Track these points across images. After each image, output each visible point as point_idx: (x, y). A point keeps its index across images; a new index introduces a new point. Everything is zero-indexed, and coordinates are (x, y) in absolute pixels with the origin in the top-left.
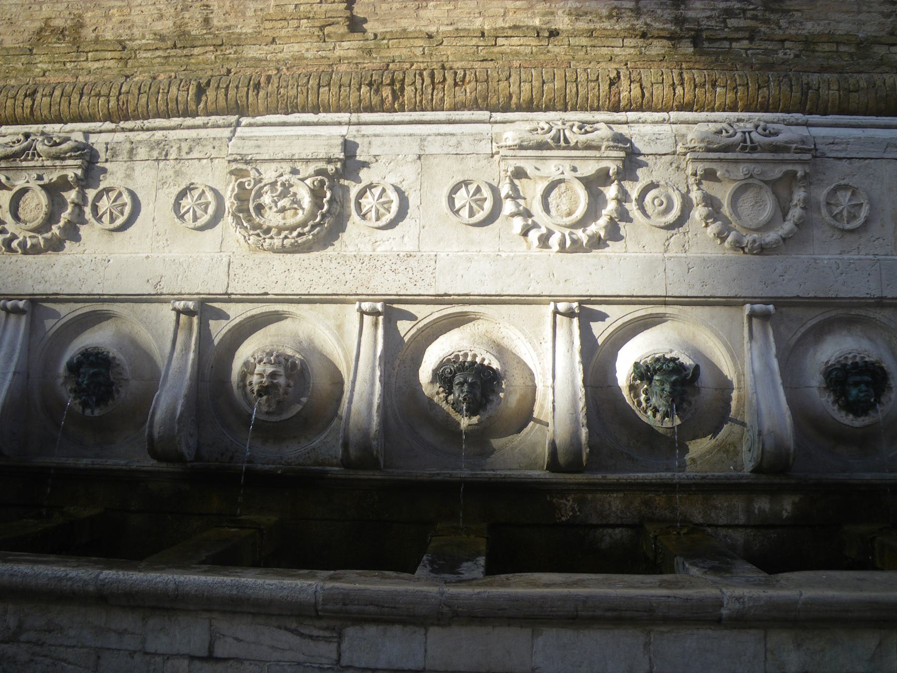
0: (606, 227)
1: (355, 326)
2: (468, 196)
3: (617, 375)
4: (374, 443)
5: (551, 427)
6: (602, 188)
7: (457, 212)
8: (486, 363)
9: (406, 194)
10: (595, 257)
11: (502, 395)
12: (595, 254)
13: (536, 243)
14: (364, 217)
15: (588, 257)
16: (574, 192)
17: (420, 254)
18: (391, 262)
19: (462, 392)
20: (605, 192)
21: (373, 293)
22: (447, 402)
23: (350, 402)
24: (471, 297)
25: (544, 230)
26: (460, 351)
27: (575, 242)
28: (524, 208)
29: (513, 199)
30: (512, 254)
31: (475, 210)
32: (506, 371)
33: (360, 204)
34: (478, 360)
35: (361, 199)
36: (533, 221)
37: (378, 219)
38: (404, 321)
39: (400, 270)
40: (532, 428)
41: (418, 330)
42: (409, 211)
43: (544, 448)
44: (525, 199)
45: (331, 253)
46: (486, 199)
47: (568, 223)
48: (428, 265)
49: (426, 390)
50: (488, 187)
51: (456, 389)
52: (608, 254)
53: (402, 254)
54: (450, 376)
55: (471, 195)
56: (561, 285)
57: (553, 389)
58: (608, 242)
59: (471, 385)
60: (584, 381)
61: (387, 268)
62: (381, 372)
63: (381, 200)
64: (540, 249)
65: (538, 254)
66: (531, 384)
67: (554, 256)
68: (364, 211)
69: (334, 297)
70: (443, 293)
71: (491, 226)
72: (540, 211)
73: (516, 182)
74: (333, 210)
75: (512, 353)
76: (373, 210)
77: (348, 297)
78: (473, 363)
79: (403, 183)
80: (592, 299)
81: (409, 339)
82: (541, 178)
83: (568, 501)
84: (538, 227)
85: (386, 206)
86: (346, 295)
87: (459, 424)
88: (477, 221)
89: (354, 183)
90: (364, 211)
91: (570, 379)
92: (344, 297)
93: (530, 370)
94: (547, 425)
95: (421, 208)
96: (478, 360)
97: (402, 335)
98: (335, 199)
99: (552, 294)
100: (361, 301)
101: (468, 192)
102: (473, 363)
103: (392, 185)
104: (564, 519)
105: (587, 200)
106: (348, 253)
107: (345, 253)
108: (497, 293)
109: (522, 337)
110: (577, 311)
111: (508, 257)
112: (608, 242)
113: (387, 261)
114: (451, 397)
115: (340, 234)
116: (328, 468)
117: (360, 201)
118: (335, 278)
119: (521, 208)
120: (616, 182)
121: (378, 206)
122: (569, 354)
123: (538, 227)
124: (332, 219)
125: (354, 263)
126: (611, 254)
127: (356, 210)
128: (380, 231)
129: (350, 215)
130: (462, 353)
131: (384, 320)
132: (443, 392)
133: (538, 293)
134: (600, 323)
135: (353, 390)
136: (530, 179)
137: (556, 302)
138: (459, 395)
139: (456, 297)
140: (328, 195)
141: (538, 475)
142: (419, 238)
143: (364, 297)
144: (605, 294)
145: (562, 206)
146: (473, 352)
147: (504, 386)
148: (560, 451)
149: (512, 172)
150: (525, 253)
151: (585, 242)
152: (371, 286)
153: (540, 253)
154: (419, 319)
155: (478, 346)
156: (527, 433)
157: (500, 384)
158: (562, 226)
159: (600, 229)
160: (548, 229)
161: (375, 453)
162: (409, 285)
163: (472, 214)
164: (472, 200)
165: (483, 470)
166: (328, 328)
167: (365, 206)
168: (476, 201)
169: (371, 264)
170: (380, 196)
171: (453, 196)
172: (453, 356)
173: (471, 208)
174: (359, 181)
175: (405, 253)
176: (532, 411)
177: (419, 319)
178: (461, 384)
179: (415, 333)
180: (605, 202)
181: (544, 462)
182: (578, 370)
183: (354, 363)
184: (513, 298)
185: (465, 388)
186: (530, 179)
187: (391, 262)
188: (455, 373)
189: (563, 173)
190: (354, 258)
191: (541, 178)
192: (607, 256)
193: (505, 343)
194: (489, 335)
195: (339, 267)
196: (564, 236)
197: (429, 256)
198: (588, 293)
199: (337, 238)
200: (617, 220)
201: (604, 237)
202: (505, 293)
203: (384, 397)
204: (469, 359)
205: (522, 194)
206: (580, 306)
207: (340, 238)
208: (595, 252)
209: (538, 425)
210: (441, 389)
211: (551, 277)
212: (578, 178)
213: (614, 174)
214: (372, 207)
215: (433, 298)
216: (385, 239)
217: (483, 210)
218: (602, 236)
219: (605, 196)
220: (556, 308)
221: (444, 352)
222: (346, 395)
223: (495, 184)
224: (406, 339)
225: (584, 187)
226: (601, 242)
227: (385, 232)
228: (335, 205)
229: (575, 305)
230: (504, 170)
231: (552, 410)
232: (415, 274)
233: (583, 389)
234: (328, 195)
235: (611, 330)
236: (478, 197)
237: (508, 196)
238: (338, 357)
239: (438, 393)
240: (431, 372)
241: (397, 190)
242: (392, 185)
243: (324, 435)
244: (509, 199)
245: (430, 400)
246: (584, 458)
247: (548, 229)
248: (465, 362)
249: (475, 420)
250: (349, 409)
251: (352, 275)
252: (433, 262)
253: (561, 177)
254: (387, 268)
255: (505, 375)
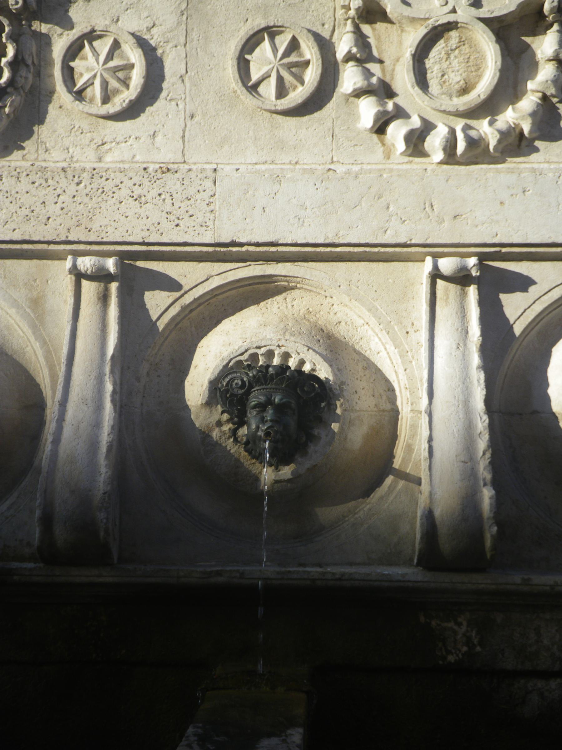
0: (533, 115)
1: (65, 301)
2: (275, 56)
3: (551, 391)
4: (101, 516)
5: (425, 487)
6: (528, 40)
7: (253, 89)
8: (307, 368)
9: (159, 52)
10: (511, 171)
11: (335, 427)
12: (512, 166)
13: (401, 146)
14: (79, 95)
15: (498, 171)
16: (475, 47)
17: (187, 167)
18: (130, 183)
19: (263, 420)
20: (534, 46)
21: (99, 240)
22: (236, 441)
23: (57, 440)
24: (280, 249)
25: (415, 122)
26: (259, 347)
27: (472, 143)
28: (379, 79)
29: (360, 62)
30: (356, 168)
31: (287, 85)
32: (343, 383)
33: (72, 70)
34: (292, 363)
35: (73, 59)
36: (396, 106)
37: (106, 100)
38: (157, 292)
39: (149, 196)
40: (392, 488)
41: (183, 308)
42: (165, 85)
43: (413, 525)
44: (381, 62)
45: (18, 164)
46: (307, 63)
47: (461, 109)
48: (201, 189)
49: (197, 417)
50: (312, 39)
51: (252, 417)
52: (536, 166)
53: (151, 167)
54: (240, 392)
55: (280, 54)
56: (446, 224)
57: (430, 415)
58: (537, 143)
59: (280, 409)
60: (488, 401)
61: (124, 192)
62: (114, 384)
63: (111, 64)
64: (407, 159)
65: (405, 167)
66: (388, 407)
67: (433, 171)
68: (80, 83)
69: (25, 246)
70: (228, 241)
71: (317, 115)
72: (409, 86)
73: (366, 29)
74: (20, 81)
75: (355, 350)
76: (97, 82)
77: (52, 247)
78: (284, 368)
79: (154, 31)
80: (504, 250)
81: (168, 325)
82: (413, 20)
83: (460, 624)
84: (407, 116)
85: (121, 75)
86: (49, 243)
87: (257, 479)
88: (292, 105)
89: (59, 30)
90: (80, 83)
91: (461, 397)
92: (45, 246)
93: (387, 381)
94: (418, 482)
95: (186, 80)
96: (292, 363)
97: (154, 318)
98: (23, 60)
99: (429, 241)
100: (76, 254)
101: (275, 50)
102: (284, 368)
103: (133, 34)
104: (451, 658)
105: (499, 63)
106: (51, 165)
107: (44, 164)
108: (327, 241)
109: (373, 321)
110: (475, 273)
111: (348, 172)
112: (537, 143)
113: (125, 180)
114: (243, 431)
115: (35, 128)
116: (15, 565)
117: (72, 64)
118: (27, 212)
119: (374, 80)
120: (556, 27)
121: (106, 75)
122: (459, 353)
123: (407, 116)
124: (19, 98)
125: (63, 183)
126: (542, 166)
127: (65, 81)
128: (110, 123)
129: (52, 92)
130: (263, 350)
131: (120, 290)
132: (228, 421)
133: (402, 240)
134: (518, 296)
135: (61, 418)
136: (391, 22)
137: (436, 256)
138: (258, 428)
139: (251, 249)
140: (11, 51)
141: (403, 575)
142: (183, 137)
143: (82, 247)
144: (529, 241)
145: (452, 75)
146: (283, 349)
147: (339, 411)
148: (443, 530)
149: (357, 10)
150: (380, 167)
151: (493, 143)
152: (95, 226)
153: (408, 166)
154: (186, 288)
155: (293, 339)
156: (382, 498)
157: (331, 407)
158: (449, 113)
159: (523, 118)
160: (424, 121)
161: (102, 534)
162: (165, 225)
163: (282, 92)
164: (283, 65)
165: (300, 565)
166: (15, 304)
167: (81, 75)
168: (289, 67)
169: (95, 186)
170: (110, 56)
171: (248, 57)
172: (246, 356)
173: (280, 80)
174: (68, 25)
175: (157, 166)
176: (391, 456)
177: (186, 288)
178: (261, 407)
179: (178, 314)
180: (534, 66)
181: (414, 551)
182: (475, 382)
183: (63, 368)
184: (356, 249)
185: (269, 414)
186: (391, 22)
187: (130, 183)
188: (251, 386)
189: (454, 11)
190: (62, 175)
191: (413, 20)
192: (533, 170)
193: (342, 332)
194: (313, 319)
195: (33, 191)
196: (452, 132)
197: (202, 170)
198: (496, 240)
199: (29, 134)
200: (555, 100)
201: (531, 132)
202: (342, 241)
203: (120, 431)
204: (276, 361)
205: (375, 53)
206: (481, 265)
207: (35, 136)
208: (512, 163)
209: (401, 483)
210: (226, 416)
211: (428, 209)
212: (483, 20)
213: (552, 11)
214: (95, 76)
215: (210, 249)
216: (120, 138)
217: (302, 83)
218: (526, 131)
219: (534, 55)
220: (436, 267)
221: (230, 349)
222: (50, 427)
223: (326, 34)
224: (161, 325)
225: (493, 38)
226: (524, 143)
227: (120, 124)
228: (23, 72)
229: (472, 261)
230: (343, 7)
231: (427, 454)
232: (177, 205)
233: (485, 418)
234: (11, 51)
235: (538, 308)
236: (293, 58)
237: (349, 57)
238: (34, 358)
239: (219, 424)
240: (206, 384)
241: (140, 19)
242: (133, 34)
243: (8, 503)
244: (351, 63)
245: (205, 436)
246: (488, 543)
247: (424, 121)
248: (268, 367)
249: (286, 472)
250: (55, 453)
251: (59, 205)
252: (208, 184)
253: (451, 18)
254: (124, 192)
255: (341, 390)
